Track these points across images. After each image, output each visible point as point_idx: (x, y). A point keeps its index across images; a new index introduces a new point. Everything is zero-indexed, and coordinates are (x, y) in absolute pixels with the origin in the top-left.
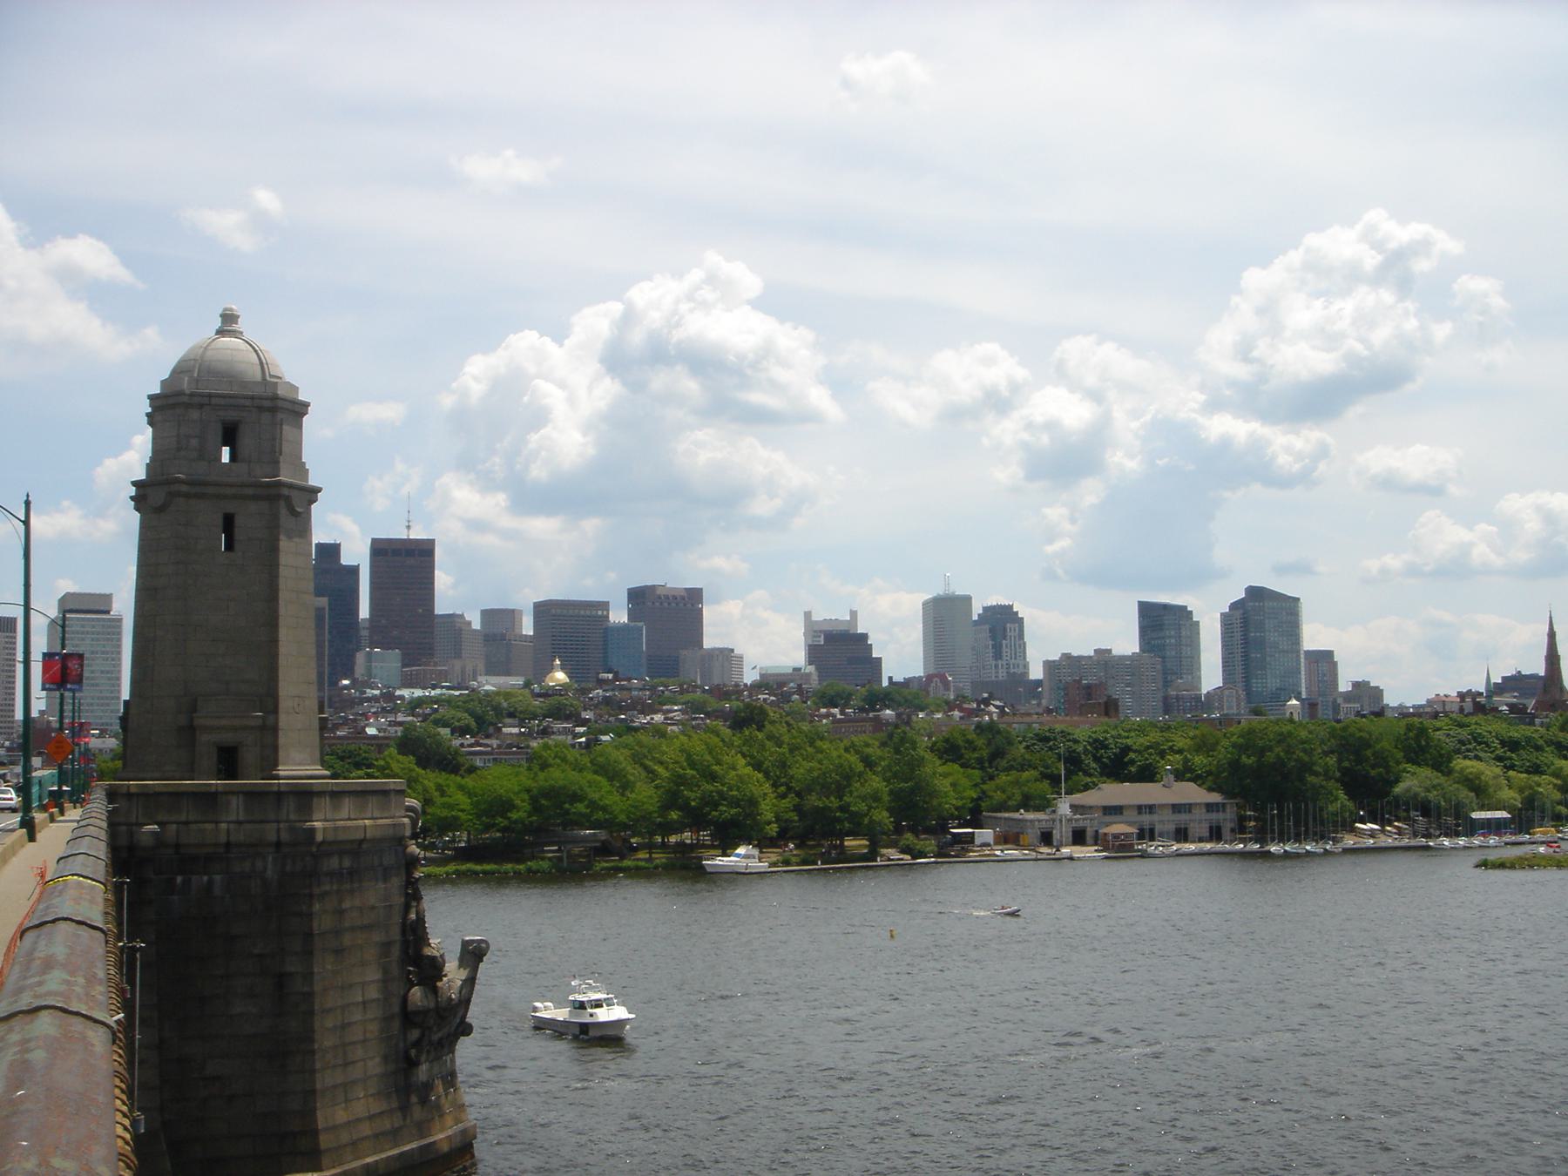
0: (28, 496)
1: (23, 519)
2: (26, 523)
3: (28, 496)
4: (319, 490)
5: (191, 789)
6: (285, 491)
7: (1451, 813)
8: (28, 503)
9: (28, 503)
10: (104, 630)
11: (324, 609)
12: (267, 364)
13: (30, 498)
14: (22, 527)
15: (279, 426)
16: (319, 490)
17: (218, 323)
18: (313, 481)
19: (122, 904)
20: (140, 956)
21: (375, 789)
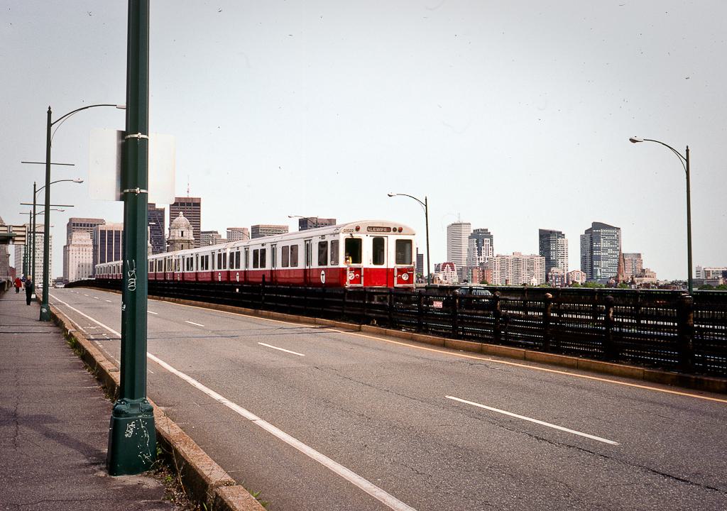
0: (50, 108)
3: (50, 108)
8: (687, 151)
9: (687, 151)
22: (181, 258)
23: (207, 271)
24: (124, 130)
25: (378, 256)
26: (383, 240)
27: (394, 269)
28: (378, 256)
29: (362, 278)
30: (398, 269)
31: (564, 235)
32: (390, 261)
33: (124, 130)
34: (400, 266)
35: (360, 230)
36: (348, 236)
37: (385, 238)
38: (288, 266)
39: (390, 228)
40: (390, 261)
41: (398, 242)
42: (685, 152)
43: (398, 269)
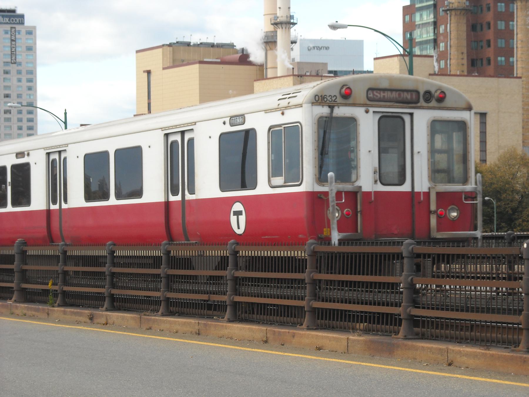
0: (65, 110)
1: (64, 121)
3: (65, 110)
4: (490, 4)
8: (66, 114)
9: (66, 114)
13: (66, 111)
16: (490, 4)
38: (106, 196)
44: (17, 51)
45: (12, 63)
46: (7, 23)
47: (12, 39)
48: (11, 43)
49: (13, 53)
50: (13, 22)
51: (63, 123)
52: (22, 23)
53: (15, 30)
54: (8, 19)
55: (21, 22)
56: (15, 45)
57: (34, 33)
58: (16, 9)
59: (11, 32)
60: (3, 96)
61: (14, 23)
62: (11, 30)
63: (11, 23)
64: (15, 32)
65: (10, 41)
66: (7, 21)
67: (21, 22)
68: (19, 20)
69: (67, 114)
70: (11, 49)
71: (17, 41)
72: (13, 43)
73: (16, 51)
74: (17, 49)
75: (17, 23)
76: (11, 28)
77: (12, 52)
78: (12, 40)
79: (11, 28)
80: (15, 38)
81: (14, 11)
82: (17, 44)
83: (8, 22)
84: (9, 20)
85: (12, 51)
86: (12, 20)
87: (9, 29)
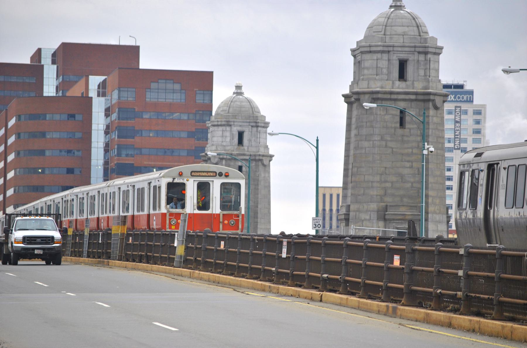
0: (317, 138)
1: (316, 146)
2: (317, 148)
3: (317, 138)
4: (273, 156)
5: (50, 247)
6: (432, 97)
7: (114, 245)
8: (317, 140)
9: (317, 140)
10: (70, 239)
11: (473, 139)
12: (254, 108)
13: (318, 138)
14: (315, 150)
15: (259, 139)
16: (273, 156)
17: (234, 90)
18: (271, 153)
19: (184, 235)
20: (13, 254)
21: (462, 190)
22: (116, 190)
23: (114, 215)
24: (145, 63)
25: (204, 204)
26: (209, 184)
27: (219, 214)
28: (204, 204)
29: (221, 220)
30: (223, 215)
31: (471, 93)
32: (215, 208)
33: (145, 63)
34: (225, 212)
35: (184, 174)
36: (170, 180)
37: (211, 183)
39: (216, 172)
40: (215, 208)
41: (223, 185)
42: (316, 141)
43: (223, 215)
44: (461, 135)
45: (455, 149)
46: (452, 101)
47: (456, 120)
48: (455, 125)
49: (456, 137)
50: (460, 100)
51: (315, 148)
52: (471, 101)
53: (460, 110)
54: (454, 96)
55: (469, 100)
56: (460, 126)
57: (483, 112)
58: (465, 83)
59: (456, 112)
60: (239, 82)
61: (461, 101)
62: (456, 109)
63: (457, 101)
64: (460, 112)
65: (453, 122)
66: (453, 98)
67: (469, 100)
68: (467, 97)
69: (319, 141)
70: (455, 133)
71: (462, 123)
72: (458, 125)
73: (460, 135)
74: (462, 132)
75: (464, 101)
76: (456, 107)
77: (455, 135)
78: (456, 122)
79: (456, 107)
80: (460, 119)
81: (461, 87)
82: (461, 125)
83: (453, 100)
84: (455, 98)
85: (456, 134)
86: (459, 98)
87: (454, 108)
